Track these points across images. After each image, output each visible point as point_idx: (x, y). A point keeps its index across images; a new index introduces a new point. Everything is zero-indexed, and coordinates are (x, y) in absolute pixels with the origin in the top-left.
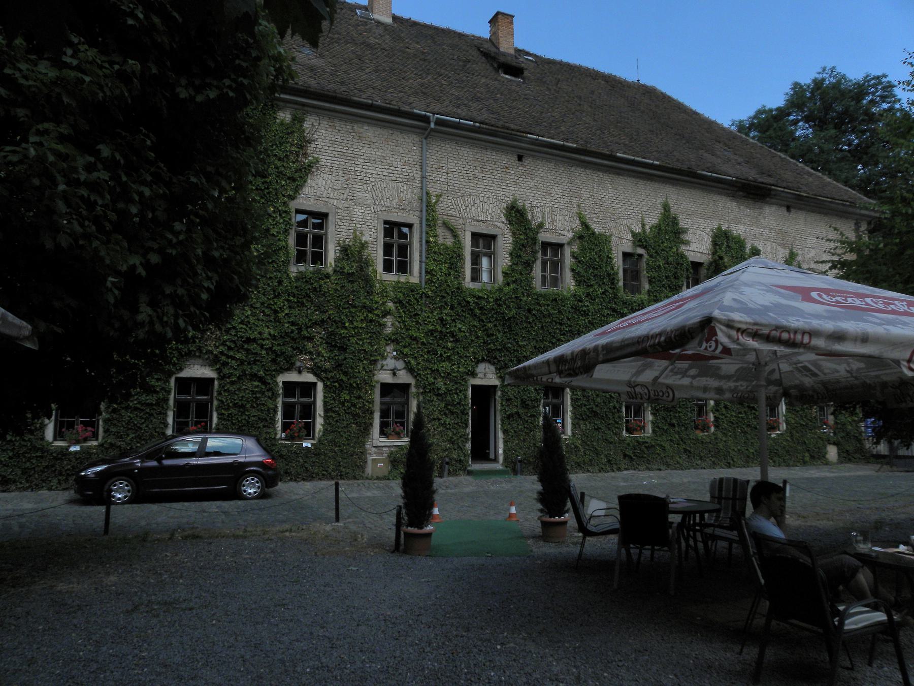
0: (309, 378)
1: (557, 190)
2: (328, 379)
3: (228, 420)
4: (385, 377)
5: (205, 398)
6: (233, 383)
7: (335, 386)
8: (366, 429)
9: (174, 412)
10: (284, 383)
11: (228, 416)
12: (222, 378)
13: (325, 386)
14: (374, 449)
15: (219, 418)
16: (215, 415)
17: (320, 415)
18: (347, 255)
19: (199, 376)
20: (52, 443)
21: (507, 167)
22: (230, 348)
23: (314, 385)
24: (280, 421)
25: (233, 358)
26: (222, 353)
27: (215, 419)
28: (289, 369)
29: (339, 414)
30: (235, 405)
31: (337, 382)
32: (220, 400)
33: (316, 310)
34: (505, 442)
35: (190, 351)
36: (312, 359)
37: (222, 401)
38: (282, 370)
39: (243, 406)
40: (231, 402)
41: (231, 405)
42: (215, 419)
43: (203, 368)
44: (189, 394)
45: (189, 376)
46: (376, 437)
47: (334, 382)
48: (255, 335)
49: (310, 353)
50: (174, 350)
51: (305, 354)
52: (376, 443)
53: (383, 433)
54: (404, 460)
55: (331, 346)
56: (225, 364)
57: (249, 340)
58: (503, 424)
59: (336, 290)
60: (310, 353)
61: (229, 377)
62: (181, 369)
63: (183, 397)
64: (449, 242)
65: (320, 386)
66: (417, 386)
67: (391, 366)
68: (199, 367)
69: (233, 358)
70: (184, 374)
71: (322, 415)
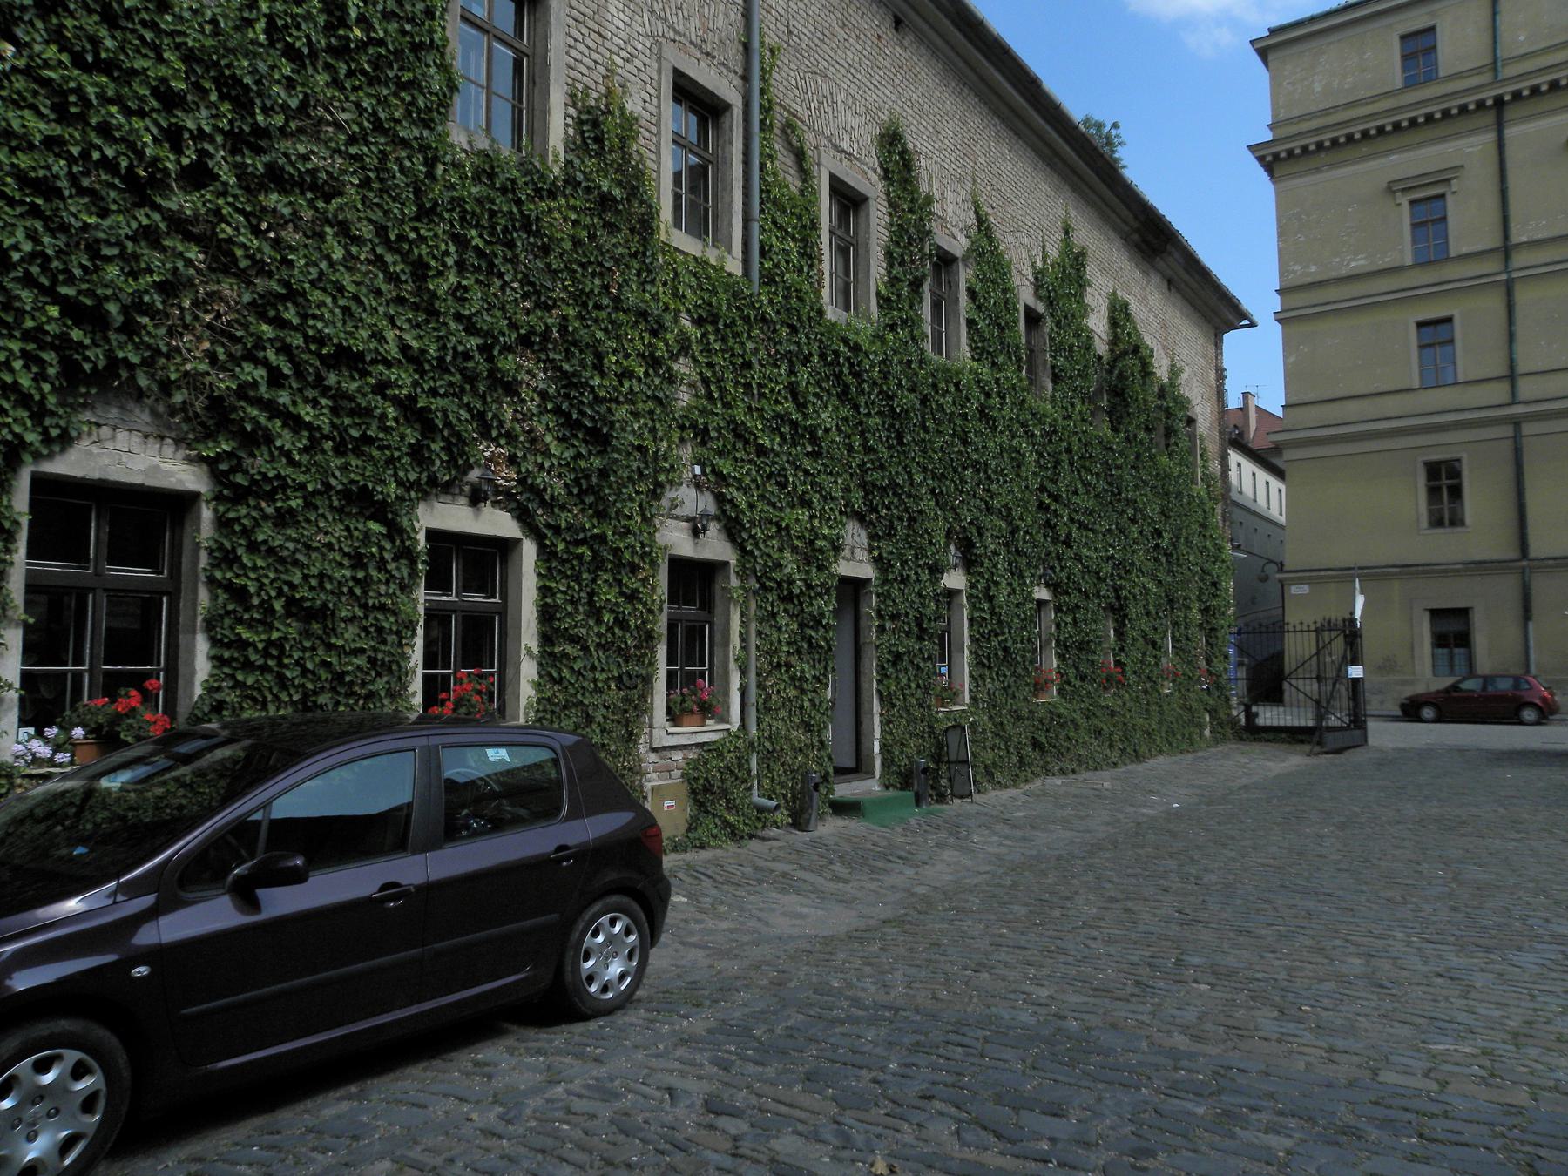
0: (497, 523)
1: (947, 128)
2: (557, 530)
3: (264, 669)
4: (676, 539)
5: (143, 573)
6: (284, 519)
7: (580, 557)
8: (637, 705)
9: (27, 629)
10: (432, 534)
11: (266, 654)
12: (229, 490)
13: (546, 553)
14: (653, 757)
15: (218, 661)
16: (202, 646)
17: (529, 650)
18: (599, 140)
19: (137, 479)
20: (287, 596)
21: (879, 37)
22: (276, 378)
23: (504, 548)
24: (420, 671)
25: (294, 423)
26: (245, 391)
27: (202, 667)
28: (447, 489)
29: (585, 649)
30: (294, 607)
31: (583, 542)
32: (228, 587)
33: (525, 296)
34: (886, 722)
35: (114, 364)
36: (512, 460)
37: (240, 594)
38: (434, 488)
39: (322, 614)
40: (280, 593)
41: (278, 606)
42: (202, 667)
43: (153, 446)
44: (81, 557)
45: (95, 475)
46: (660, 729)
47: (578, 543)
48: (360, 341)
49: (511, 437)
50: (43, 346)
51: (495, 440)
52: (661, 739)
53: (674, 717)
54: (1106, 150)
55: (570, 425)
56: (256, 439)
57: (346, 359)
58: (883, 677)
59: (577, 242)
60: (511, 437)
61: (270, 497)
62: (65, 440)
63: (53, 567)
64: (794, 183)
65: (529, 550)
66: (743, 574)
67: (688, 509)
68: (136, 438)
69: (294, 423)
70: (69, 464)
71: (536, 650)
